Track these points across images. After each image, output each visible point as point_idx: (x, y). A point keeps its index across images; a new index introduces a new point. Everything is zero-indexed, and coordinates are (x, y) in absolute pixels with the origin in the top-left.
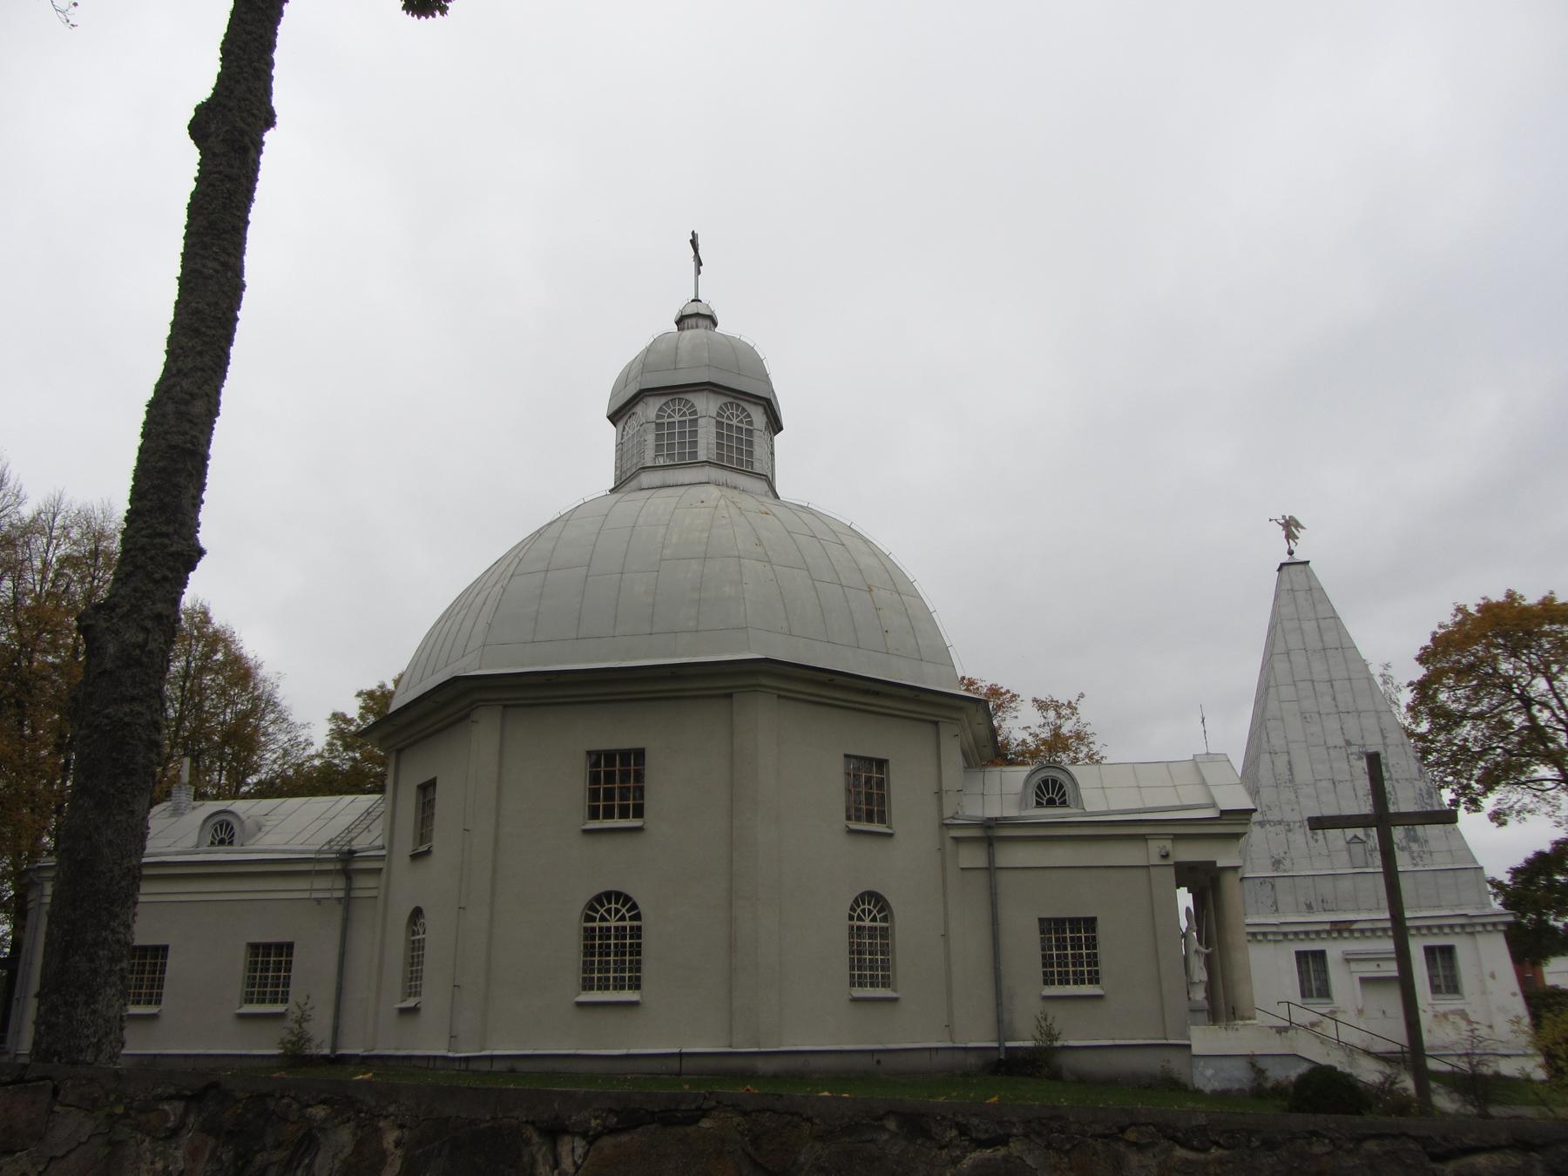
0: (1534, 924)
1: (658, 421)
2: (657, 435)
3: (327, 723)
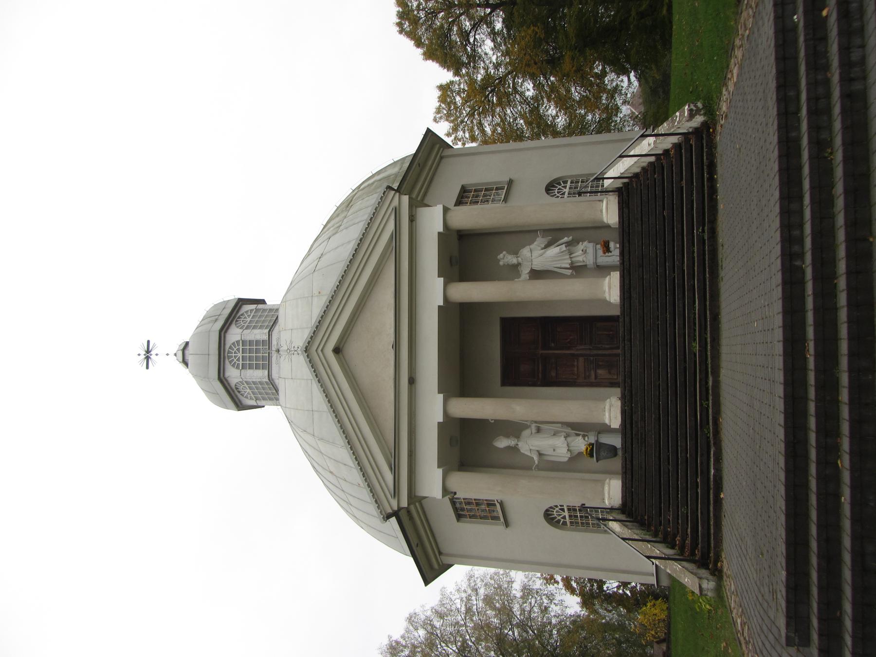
0: (581, 76)
1: (241, 368)
2: (249, 369)
3: (439, 469)
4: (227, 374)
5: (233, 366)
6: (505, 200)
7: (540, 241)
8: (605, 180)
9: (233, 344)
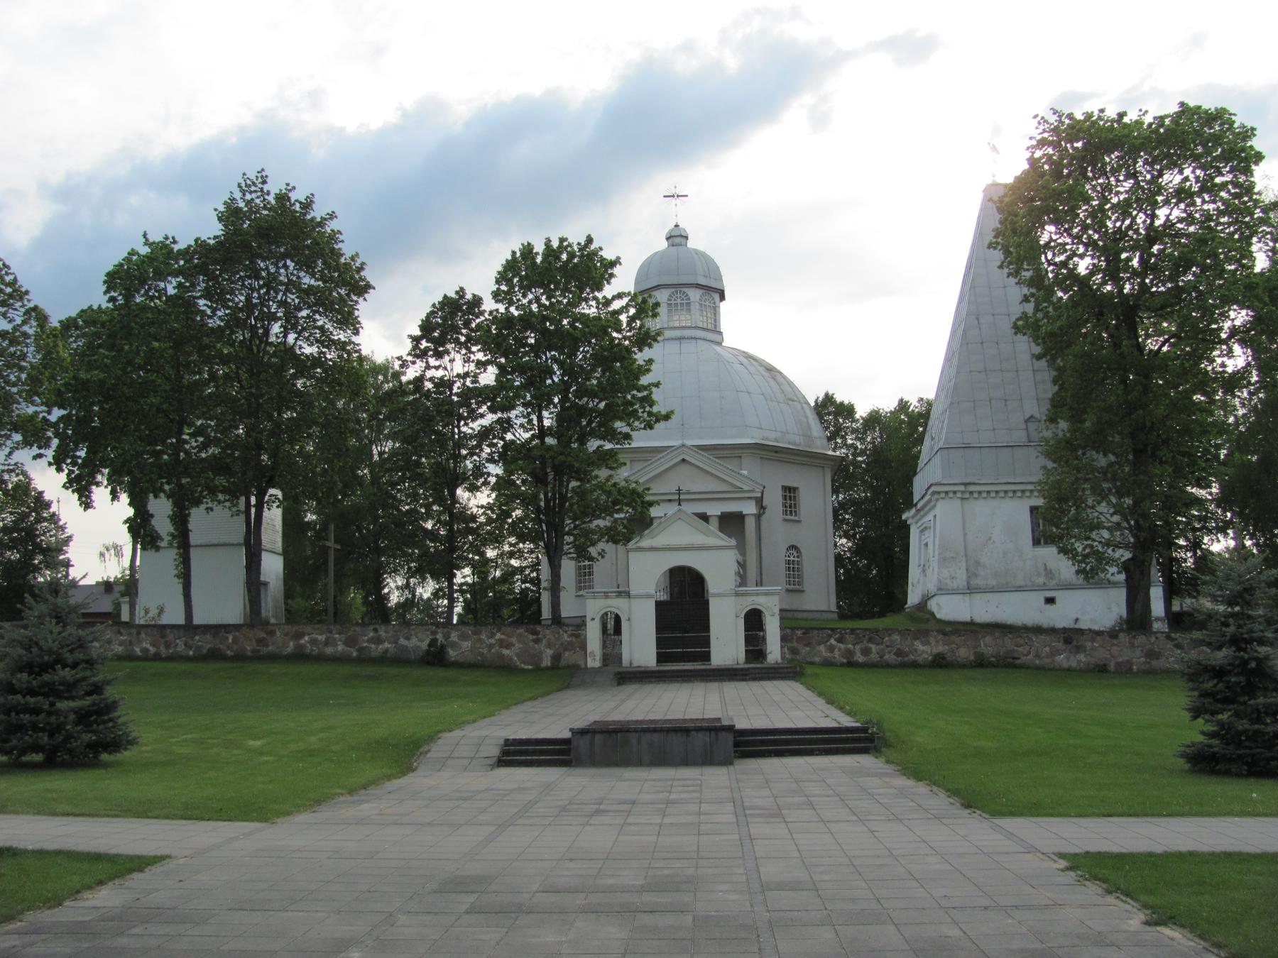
4: (663, 291)
5: (670, 296)
6: (785, 520)
7: (740, 558)
8: (564, 613)
9: (687, 295)
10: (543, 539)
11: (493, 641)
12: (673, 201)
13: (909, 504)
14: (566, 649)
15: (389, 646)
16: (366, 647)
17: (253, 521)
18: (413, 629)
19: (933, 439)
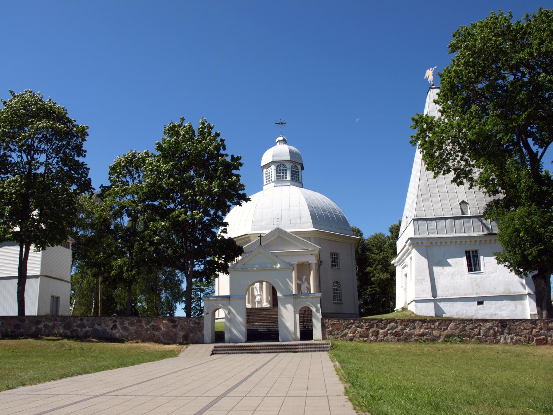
10: (27, 190)
11: (148, 326)
12: (280, 126)
13: (395, 254)
14: (191, 332)
15: (89, 329)
16: (76, 329)
17: (23, 255)
18: (103, 319)
19: (407, 218)
